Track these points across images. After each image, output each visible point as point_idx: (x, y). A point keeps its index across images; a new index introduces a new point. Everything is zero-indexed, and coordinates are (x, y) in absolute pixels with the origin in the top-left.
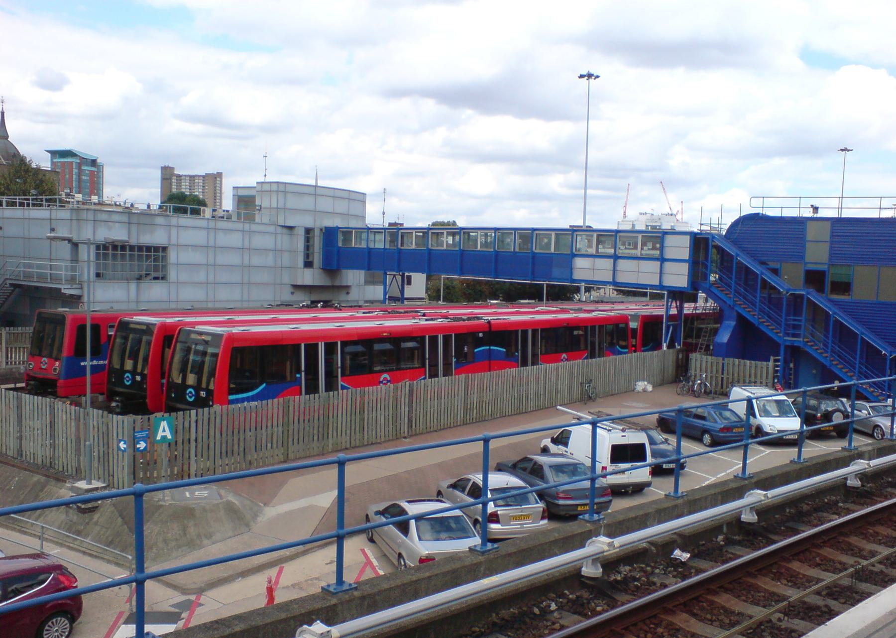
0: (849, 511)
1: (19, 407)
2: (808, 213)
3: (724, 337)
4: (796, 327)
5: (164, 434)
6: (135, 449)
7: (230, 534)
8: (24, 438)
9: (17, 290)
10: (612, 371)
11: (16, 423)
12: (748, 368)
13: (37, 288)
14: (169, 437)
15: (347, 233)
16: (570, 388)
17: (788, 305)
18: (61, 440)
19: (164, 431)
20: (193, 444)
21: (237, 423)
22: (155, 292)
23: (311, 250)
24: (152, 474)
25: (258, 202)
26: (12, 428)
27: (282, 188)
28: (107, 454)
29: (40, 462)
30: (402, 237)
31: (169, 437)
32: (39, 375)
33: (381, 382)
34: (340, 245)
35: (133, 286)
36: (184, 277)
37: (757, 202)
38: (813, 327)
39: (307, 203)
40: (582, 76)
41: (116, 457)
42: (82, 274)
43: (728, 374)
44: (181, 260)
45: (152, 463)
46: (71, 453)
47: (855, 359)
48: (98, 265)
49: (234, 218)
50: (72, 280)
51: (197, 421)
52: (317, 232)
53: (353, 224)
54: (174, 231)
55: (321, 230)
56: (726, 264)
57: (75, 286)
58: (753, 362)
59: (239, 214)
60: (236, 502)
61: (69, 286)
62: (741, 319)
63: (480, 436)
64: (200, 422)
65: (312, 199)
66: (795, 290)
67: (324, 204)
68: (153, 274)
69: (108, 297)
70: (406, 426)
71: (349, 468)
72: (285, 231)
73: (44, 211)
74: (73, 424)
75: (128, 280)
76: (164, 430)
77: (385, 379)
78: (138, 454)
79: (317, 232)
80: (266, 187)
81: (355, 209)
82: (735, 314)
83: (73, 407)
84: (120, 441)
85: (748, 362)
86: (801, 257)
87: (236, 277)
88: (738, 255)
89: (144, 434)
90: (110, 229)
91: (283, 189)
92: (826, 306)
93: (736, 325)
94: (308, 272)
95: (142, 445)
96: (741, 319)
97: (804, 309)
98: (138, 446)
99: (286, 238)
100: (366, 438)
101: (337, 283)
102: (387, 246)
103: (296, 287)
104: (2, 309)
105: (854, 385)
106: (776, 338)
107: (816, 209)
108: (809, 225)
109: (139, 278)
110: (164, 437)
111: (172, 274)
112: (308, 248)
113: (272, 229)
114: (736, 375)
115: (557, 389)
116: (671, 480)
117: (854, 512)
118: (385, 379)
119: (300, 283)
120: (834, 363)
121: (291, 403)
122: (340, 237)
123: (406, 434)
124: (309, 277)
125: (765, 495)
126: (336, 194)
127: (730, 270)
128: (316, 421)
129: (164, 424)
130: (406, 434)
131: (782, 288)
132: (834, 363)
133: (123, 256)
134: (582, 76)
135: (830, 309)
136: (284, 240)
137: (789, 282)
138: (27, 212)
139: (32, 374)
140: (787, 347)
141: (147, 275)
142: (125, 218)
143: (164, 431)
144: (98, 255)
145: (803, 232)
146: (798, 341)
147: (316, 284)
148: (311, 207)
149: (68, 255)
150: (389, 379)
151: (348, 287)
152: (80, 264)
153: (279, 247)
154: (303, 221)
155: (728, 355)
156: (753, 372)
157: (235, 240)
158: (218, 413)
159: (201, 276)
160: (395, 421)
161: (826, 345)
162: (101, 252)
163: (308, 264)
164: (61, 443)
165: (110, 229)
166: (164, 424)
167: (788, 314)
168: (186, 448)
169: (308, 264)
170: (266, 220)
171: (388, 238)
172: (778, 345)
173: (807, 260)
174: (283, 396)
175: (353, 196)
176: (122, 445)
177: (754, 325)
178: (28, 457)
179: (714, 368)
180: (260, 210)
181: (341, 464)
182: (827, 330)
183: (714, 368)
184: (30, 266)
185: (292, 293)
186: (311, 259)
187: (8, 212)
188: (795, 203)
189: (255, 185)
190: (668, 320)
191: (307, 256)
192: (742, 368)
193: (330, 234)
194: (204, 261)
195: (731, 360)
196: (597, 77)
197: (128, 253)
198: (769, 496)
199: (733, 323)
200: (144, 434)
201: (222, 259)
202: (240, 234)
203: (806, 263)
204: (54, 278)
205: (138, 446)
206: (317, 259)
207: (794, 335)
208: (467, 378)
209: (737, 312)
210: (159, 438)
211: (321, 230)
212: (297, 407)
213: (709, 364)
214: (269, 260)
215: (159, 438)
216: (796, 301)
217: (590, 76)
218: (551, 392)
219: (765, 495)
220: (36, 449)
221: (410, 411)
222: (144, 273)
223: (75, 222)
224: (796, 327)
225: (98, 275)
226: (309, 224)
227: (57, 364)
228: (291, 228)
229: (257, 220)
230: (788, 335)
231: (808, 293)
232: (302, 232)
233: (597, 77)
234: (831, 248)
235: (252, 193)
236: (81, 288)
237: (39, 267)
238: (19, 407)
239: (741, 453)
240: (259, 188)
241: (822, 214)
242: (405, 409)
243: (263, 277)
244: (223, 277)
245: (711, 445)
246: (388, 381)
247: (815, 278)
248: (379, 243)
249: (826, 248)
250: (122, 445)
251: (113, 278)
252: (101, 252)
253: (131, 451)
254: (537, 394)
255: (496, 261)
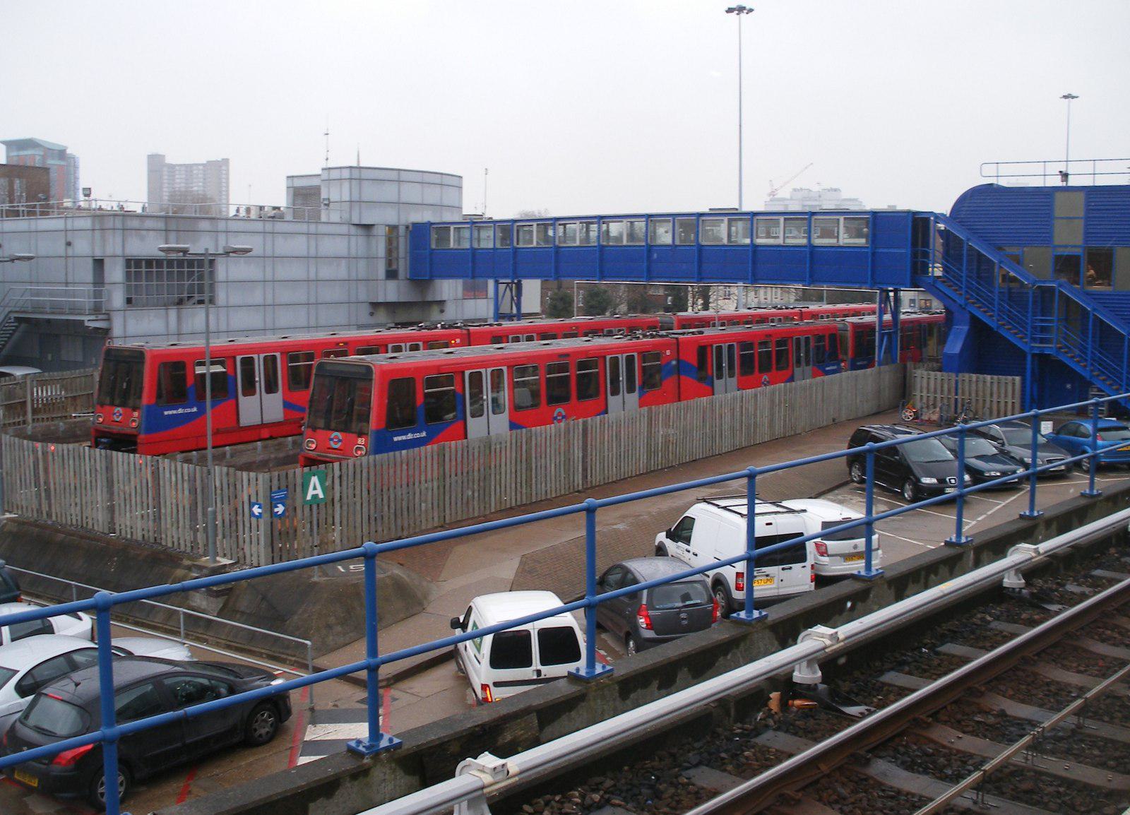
0: (1112, 582)
1: (109, 469)
2: (1057, 182)
3: (955, 346)
4: (1044, 330)
5: (315, 492)
6: (273, 514)
7: (402, 615)
8: (117, 508)
9: (23, 326)
10: (820, 397)
11: (105, 490)
12: (988, 385)
13: (48, 321)
14: (321, 496)
15: (443, 228)
16: (771, 421)
17: (1035, 302)
18: (167, 510)
19: (315, 488)
20: (337, 506)
21: (386, 477)
22: (196, 318)
23: (394, 255)
24: (292, 545)
25: (324, 195)
26: (100, 496)
27: (356, 174)
28: (234, 523)
29: (140, 538)
30: (518, 231)
31: (321, 496)
32: (116, 429)
33: (555, 418)
34: (433, 246)
35: (173, 313)
36: (235, 299)
37: (991, 170)
38: (1065, 327)
39: (389, 192)
40: (730, 10)
41: (247, 525)
42: (109, 300)
43: (963, 394)
44: (232, 277)
45: (291, 532)
46: (184, 521)
47: (1122, 368)
48: (128, 288)
49: (289, 217)
50: (97, 309)
51: (340, 477)
52: (402, 231)
53: (448, 217)
54: (222, 238)
55: (407, 227)
56: (952, 252)
57: (100, 317)
58: (995, 377)
59: (295, 212)
60: (404, 576)
61: (93, 317)
62: (975, 322)
63: (745, 472)
64: (345, 478)
65: (394, 187)
66: (1045, 282)
67: (411, 193)
68: (197, 297)
69: (145, 330)
70: (580, 477)
71: (600, 516)
72: (360, 231)
73: (54, 222)
74: (186, 485)
75: (166, 305)
76: (315, 488)
77: (336, 437)
78: (276, 520)
79: (402, 231)
80: (335, 174)
81: (449, 197)
82: (968, 316)
83: (186, 466)
84: (251, 505)
85: (988, 377)
86: (1047, 239)
87: (300, 295)
88: (968, 240)
89: (282, 494)
90: (142, 239)
91: (358, 175)
92: (1083, 301)
93: (969, 330)
94: (392, 285)
95: (280, 509)
96: (975, 322)
97: (1056, 305)
98: (276, 510)
99: (362, 241)
100: (534, 493)
101: (430, 298)
102: (498, 245)
103: (375, 305)
104: (4, 352)
105: (870, 451)
106: (1019, 344)
107: (1065, 176)
108: (1058, 195)
109: (180, 302)
110: (315, 497)
111: (221, 296)
112: (390, 251)
113: (344, 229)
114: (973, 395)
115: (755, 423)
116: (950, 517)
117: (1120, 581)
118: (560, 414)
119: (381, 300)
120: (1095, 373)
121: (447, 449)
122: (434, 236)
123: (580, 488)
124: (392, 292)
125: (834, 637)
126: (426, 179)
127: (959, 259)
128: (476, 474)
129: (315, 480)
130: (580, 488)
131: (1027, 280)
132: (1095, 373)
133: (159, 275)
134: (730, 10)
135: (1088, 305)
136: (358, 244)
137: (1034, 268)
138: (33, 222)
139: (102, 427)
140: (1034, 355)
141: (189, 298)
142: (161, 225)
143: (315, 488)
144: (128, 275)
145: (1050, 206)
146: (1049, 348)
147: (402, 300)
148: (394, 198)
149: (89, 277)
150: (564, 413)
151: (442, 303)
152: (107, 287)
153: (353, 253)
154: (382, 217)
155: (959, 370)
156: (995, 389)
157: (298, 246)
158: (365, 464)
159: (257, 297)
160: (567, 471)
161: (1083, 350)
162: (133, 270)
163: (391, 274)
164: (169, 510)
165: (142, 239)
166: (315, 480)
167: (1035, 314)
168: (330, 511)
169: (391, 274)
170: (335, 217)
171: (499, 235)
172: (1023, 355)
173: (1056, 243)
174: (438, 442)
175: (446, 180)
176: (256, 510)
177: (991, 329)
178: (123, 532)
179: (946, 386)
180: (327, 205)
181: (590, 511)
182: (1084, 332)
183: (946, 386)
184: (38, 293)
185: (372, 314)
186: (394, 267)
187: (10, 225)
188: (1039, 169)
189: (319, 172)
190: (881, 329)
191: (389, 263)
192: (981, 385)
193: (419, 232)
194: (259, 276)
195: (967, 376)
196: (751, 10)
197: (165, 270)
198: (841, 636)
199: (966, 328)
200: (282, 494)
201: (284, 272)
202: (304, 238)
203: (1055, 247)
204: (74, 309)
205: (276, 510)
206: (403, 267)
207: (1042, 341)
208: (650, 411)
209: (970, 312)
210: (309, 498)
211: (407, 227)
212: (453, 457)
213: (939, 381)
214: (342, 272)
215: (309, 498)
216: (1045, 295)
217: (741, 9)
218: (748, 427)
219: (1036, 551)
220: (133, 523)
221: (584, 457)
222: (185, 295)
223: (97, 233)
224: (1044, 330)
225: (129, 301)
226: (393, 220)
227: (136, 414)
228: (368, 227)
229: (324, 219)
230: (1034, 340)
231: (1061, 286)
232: (381, 231)
233: (751, 10)
234: (1086, 226)
235: (315, 182)
236: (109, 320)
237: (51, 294)
238: (109, 469)
239: (955, 511)
240: (325, 176)
241: (1073, 182)
242: (578, 454)
243: (336, 293)
244: (285, 296)
245: (913, 500)
246: (564, 417)
247: (1067, 265)
248: (487, 240)
249: (1080, 225)
250: (256, 510)
251: (147, 305)
252: (133, 270)
253: (267, 516)
254: (732, 429)
255: (601, 260)
